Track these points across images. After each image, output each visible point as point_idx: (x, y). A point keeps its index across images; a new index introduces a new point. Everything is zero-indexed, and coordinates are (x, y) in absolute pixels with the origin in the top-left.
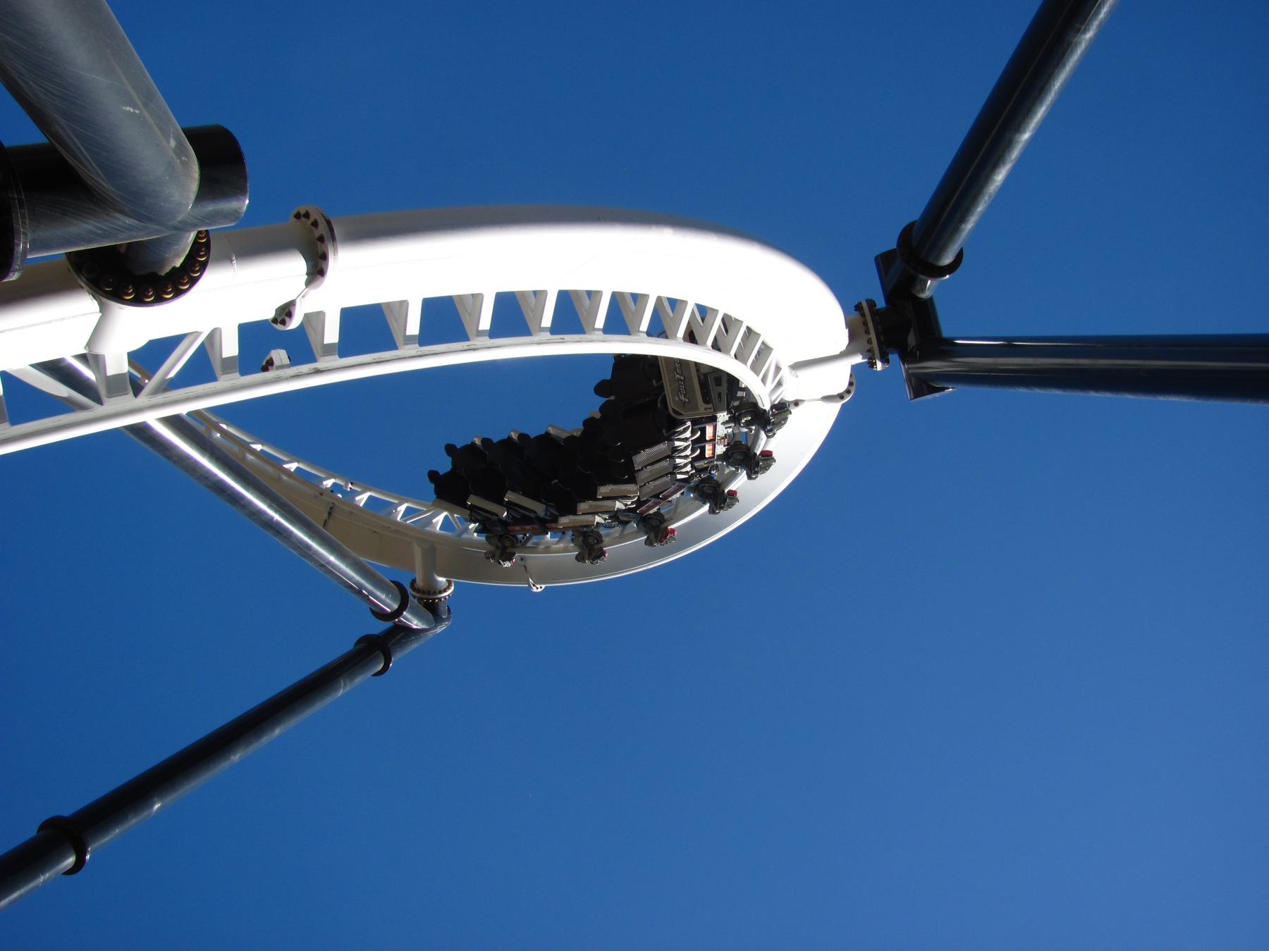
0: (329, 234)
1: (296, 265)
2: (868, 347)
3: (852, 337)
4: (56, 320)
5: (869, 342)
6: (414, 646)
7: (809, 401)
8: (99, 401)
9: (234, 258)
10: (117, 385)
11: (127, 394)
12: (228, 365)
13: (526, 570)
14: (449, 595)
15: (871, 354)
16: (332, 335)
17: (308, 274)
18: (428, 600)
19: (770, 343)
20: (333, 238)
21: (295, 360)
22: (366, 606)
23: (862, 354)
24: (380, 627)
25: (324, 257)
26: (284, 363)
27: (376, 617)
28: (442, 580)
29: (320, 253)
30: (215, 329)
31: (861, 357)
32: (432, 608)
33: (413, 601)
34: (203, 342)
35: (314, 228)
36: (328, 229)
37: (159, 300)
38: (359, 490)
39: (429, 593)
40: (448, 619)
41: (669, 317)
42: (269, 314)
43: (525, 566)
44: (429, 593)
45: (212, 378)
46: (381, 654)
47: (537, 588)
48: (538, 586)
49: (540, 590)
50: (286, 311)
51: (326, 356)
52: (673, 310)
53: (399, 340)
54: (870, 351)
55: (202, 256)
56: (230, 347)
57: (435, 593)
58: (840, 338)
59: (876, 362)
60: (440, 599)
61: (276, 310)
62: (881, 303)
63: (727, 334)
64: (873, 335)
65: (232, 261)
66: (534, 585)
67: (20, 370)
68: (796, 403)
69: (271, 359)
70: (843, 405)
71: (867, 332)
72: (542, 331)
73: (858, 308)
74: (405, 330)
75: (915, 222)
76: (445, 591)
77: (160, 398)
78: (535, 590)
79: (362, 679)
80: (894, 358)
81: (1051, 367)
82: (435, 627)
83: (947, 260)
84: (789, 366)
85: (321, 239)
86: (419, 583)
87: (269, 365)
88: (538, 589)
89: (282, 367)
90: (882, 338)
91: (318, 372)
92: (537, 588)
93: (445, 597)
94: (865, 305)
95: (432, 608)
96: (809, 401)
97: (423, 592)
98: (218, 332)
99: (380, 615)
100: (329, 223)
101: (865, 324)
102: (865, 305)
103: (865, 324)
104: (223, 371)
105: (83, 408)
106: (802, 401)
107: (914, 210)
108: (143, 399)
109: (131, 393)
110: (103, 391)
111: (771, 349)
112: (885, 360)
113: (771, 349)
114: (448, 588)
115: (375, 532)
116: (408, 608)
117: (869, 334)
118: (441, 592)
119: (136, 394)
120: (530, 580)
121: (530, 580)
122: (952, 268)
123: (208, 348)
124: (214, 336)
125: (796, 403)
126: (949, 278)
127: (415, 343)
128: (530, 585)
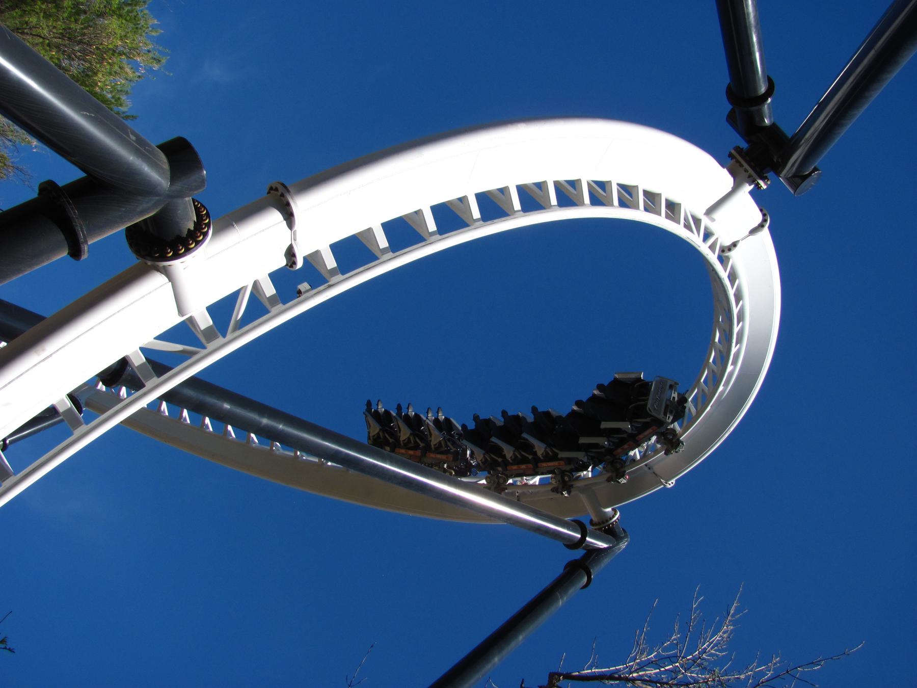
0: (285, 190)
1: (275, 217)
2: (747, 174)
3: (732, 172)
4: (146, 295)
5: (746, 171)
6: (606, 561)
7: (743, 239)
8: (204, 347)
9: (234, 224)
10: (210, 334)
11: (219, 337)
12: (273, 300)
13: (656, 474)
14: (618, 519)
15: (751, 179)
16: (330, 262)
17: (285, 219)
18: (605, 527)
19: (675, 199)
20: (288, 191)
21: (313, 287)
22: (560, 544)
23: (748, 183)
24: (578, 554)
25: (288, 204)
26: (307, 289)
27: (568, 548)
28: (609, 509)
29: (285, 203)
30: (255, 281)
31: (747, 185)
32: (609, 531)
33: (589, 528)
34: (251, 292)
35: (282, 198)
36: (283, 188)
37: (188, 250)
38: (129, 130)
39: (603, 523)
40: (626, 536)
41: (574, 194)
42: (282, 262)
43: (654, 473)
44: (603, 523)
45: (267, 311)
46: (584, 573)
47: (670, 484)
48: (670, 483)
49: (672, 485)
50: (290, 254)
51: (333, 276)
52: (575, 189)
53: (378, 254)
54: (750, 176)
55: (205, 220)
56: (269, 290)
57: (607, 521)
58: (725, 179)
59: (758, 182)
60: (612, 523)
61: (285, 255)
62: (744, 145)
63: (632, 197)
64: (746, 166)
65: (233, 226)
66: (666, 483)
67: (148, 343)
68: (734, 245)
69: (300, 290)
70: (769, 228)
71: (741, 165)
72: (477, 222)
73: (731, 156)
74: (378, 246)
75: (729, 85)
76: (613, 517)
77: (238, 333)
78: (669, 486)
79: (574, 591)
80: (771, 175)
81: (850, 88)
82: (618, 544)
83: (763, 89)
84: (704, 214)
85: (282, 195)
86: (595, 519)
87: (299, 293)
88: (671, 483)
89: (307, 291)
90: (752, 164)
91: (330, 286)
92: (670, 484)
93: (615, 521)
94: (733, 151)
95: (609, 531)
96: (743, 239)
97: (599, 524)
98: (257, 282)
99: (573, 545)
100: (283, 185)
101: (737, 161)
102: (733, 151)
103: (737, 161)
104: (271, 306)
105: (194, 353)
106: (738, 241)
107: (723, 78)
108: (229, 336)
109: (221, 337)
110: (203, 341)
111: (680, 204)
112: (764, 178)
113: (680, 204)
114: (615, 514)
115: (552, 499)
116: (588, 534)
117: (743, 166)
118: (611, 519)
119: (224, 336)
120: (662, 480)
121: (662, 480)
122: (770, 92)
123: (255, 293)
124: (256, 285)
125: (734, 245)
126: (772, 101)
127: (389, 252)
128: (664, 485)
